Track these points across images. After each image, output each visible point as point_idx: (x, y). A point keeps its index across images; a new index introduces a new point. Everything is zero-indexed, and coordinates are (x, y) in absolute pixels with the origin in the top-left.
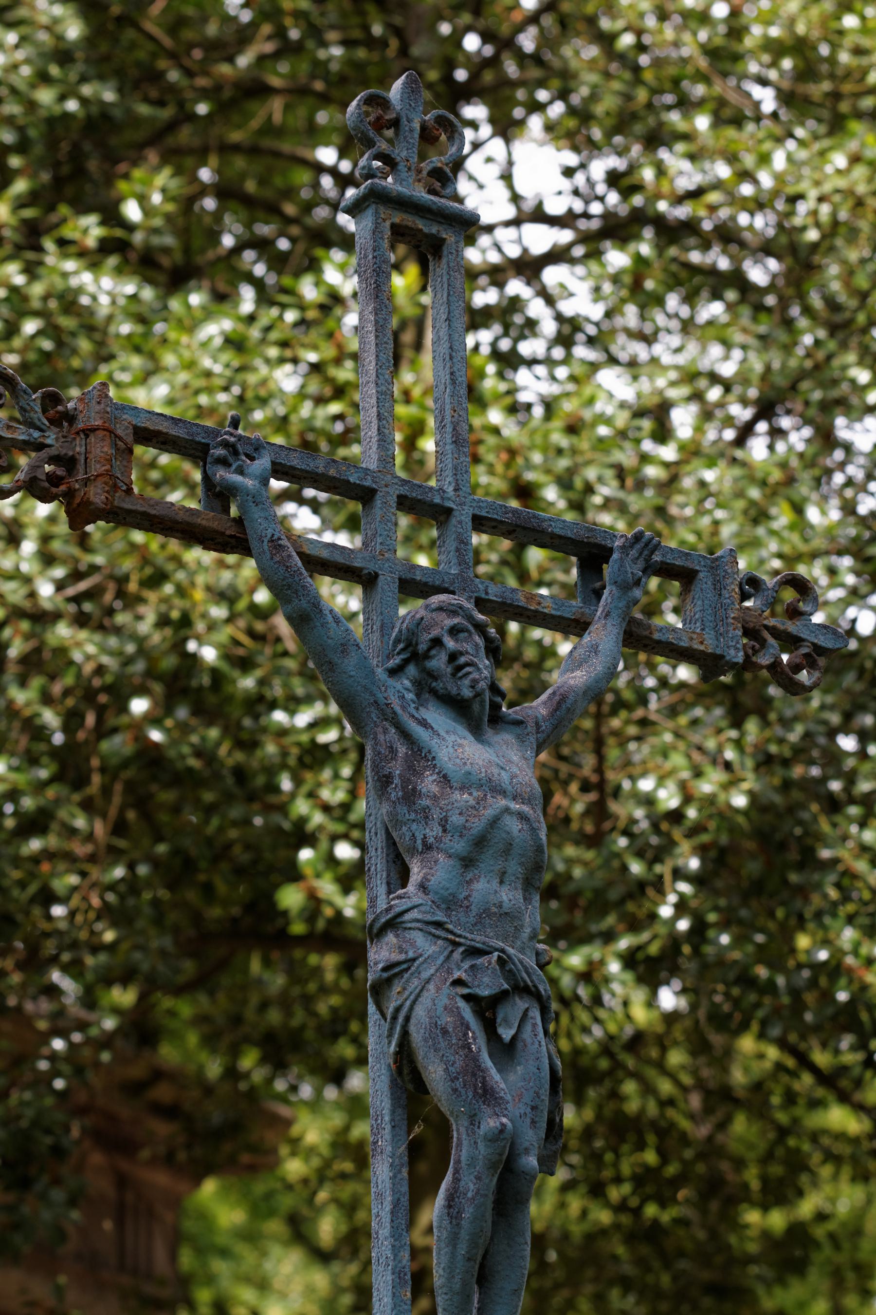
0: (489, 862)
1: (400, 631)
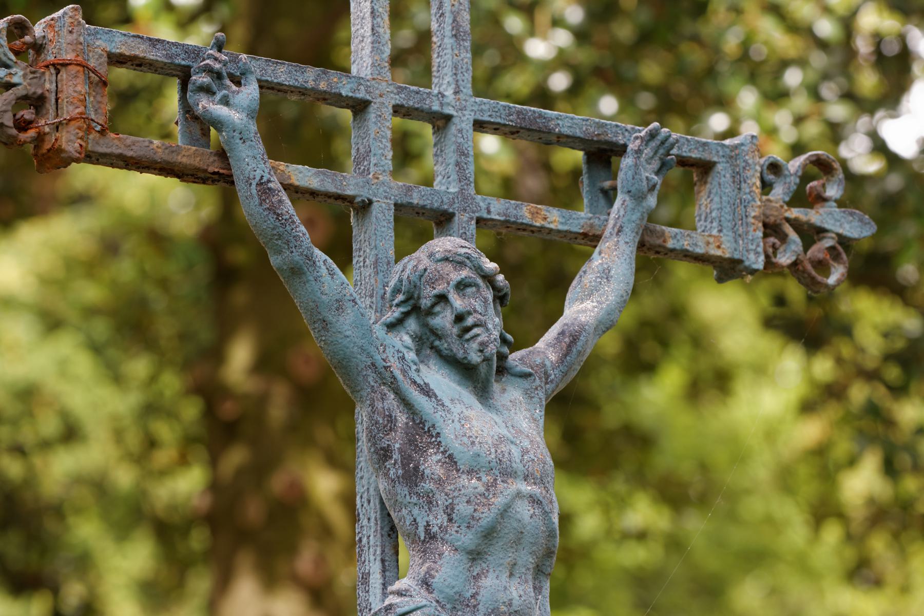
0: (499, 555)
1: (400, 281)
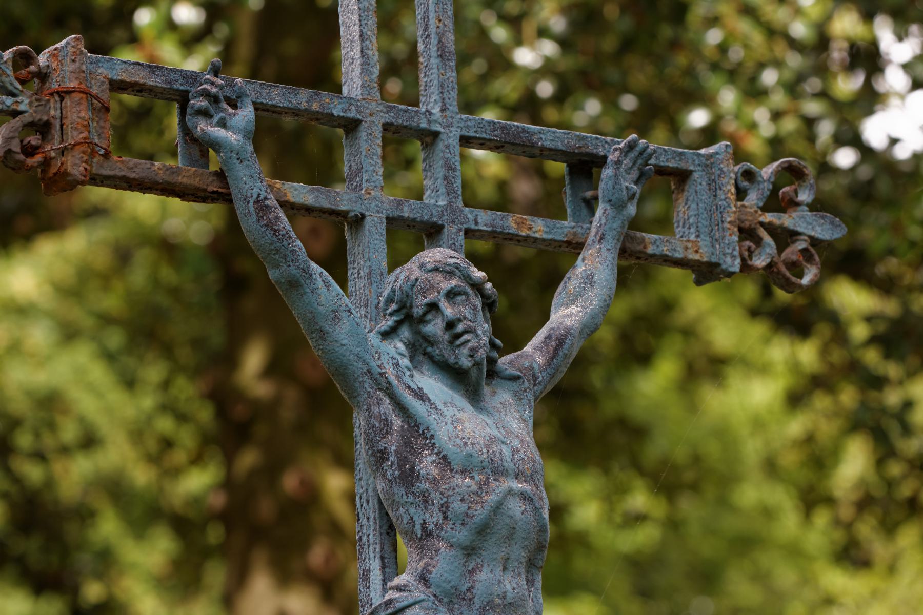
1: (393, 291)
